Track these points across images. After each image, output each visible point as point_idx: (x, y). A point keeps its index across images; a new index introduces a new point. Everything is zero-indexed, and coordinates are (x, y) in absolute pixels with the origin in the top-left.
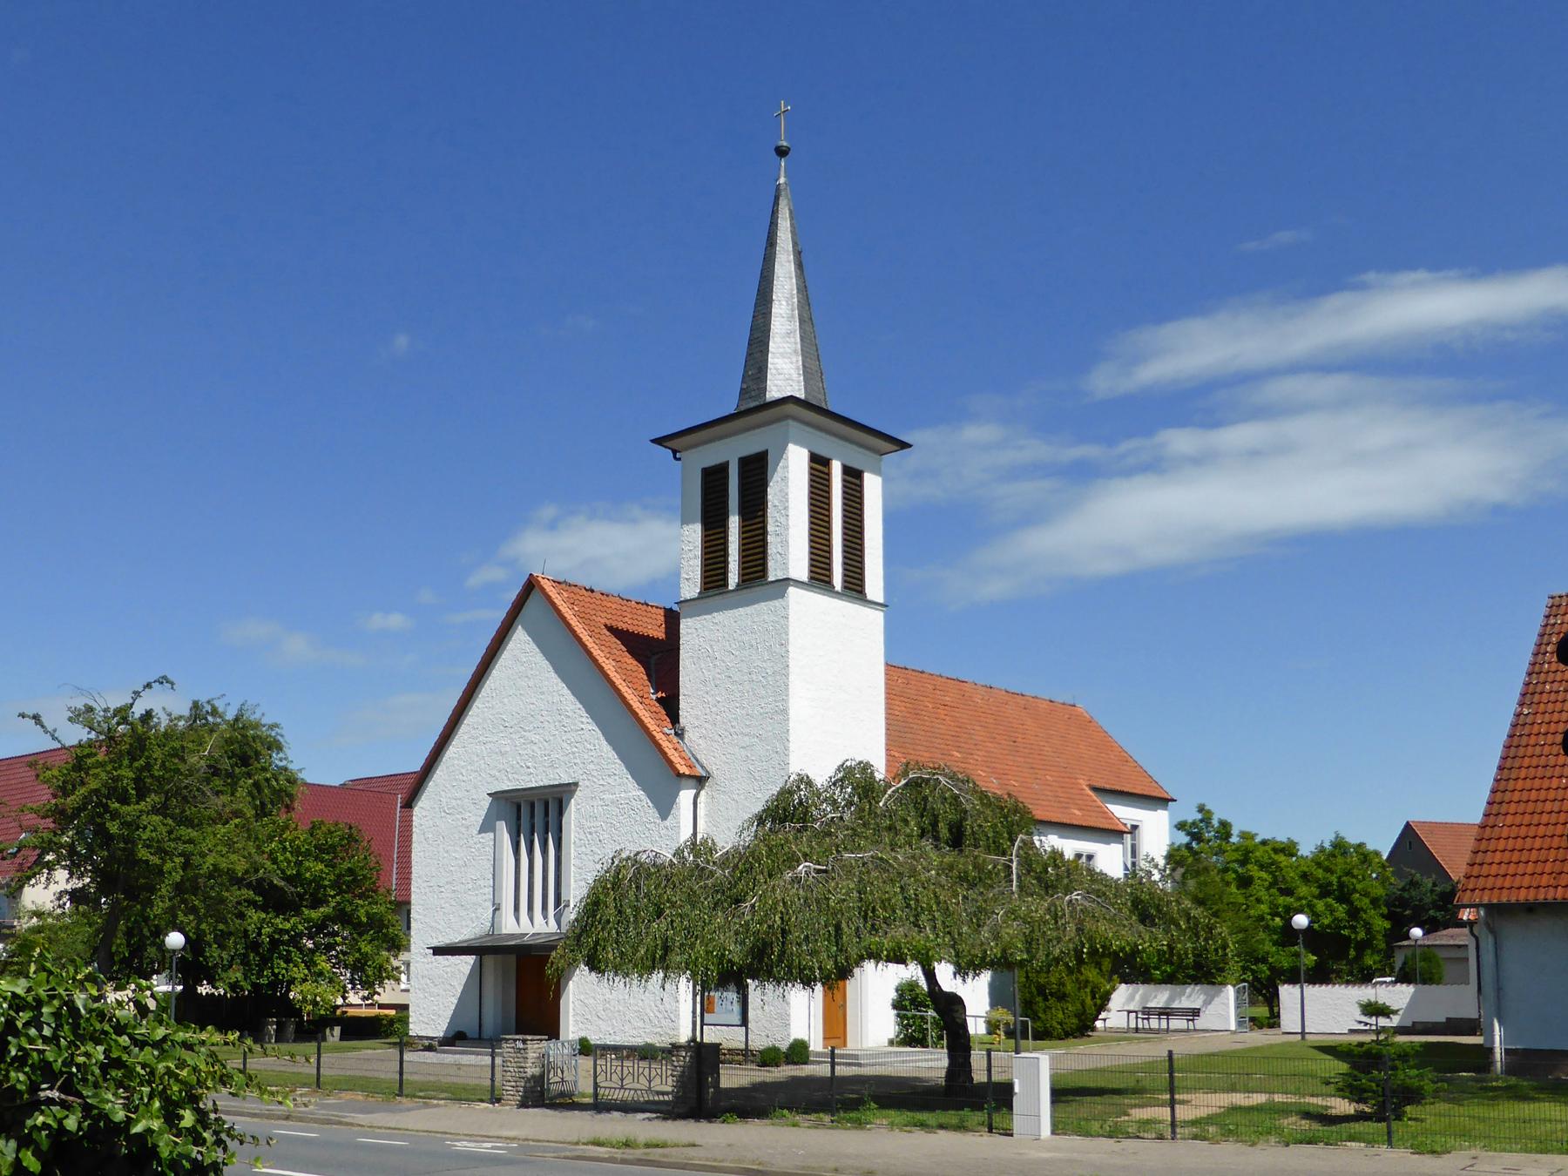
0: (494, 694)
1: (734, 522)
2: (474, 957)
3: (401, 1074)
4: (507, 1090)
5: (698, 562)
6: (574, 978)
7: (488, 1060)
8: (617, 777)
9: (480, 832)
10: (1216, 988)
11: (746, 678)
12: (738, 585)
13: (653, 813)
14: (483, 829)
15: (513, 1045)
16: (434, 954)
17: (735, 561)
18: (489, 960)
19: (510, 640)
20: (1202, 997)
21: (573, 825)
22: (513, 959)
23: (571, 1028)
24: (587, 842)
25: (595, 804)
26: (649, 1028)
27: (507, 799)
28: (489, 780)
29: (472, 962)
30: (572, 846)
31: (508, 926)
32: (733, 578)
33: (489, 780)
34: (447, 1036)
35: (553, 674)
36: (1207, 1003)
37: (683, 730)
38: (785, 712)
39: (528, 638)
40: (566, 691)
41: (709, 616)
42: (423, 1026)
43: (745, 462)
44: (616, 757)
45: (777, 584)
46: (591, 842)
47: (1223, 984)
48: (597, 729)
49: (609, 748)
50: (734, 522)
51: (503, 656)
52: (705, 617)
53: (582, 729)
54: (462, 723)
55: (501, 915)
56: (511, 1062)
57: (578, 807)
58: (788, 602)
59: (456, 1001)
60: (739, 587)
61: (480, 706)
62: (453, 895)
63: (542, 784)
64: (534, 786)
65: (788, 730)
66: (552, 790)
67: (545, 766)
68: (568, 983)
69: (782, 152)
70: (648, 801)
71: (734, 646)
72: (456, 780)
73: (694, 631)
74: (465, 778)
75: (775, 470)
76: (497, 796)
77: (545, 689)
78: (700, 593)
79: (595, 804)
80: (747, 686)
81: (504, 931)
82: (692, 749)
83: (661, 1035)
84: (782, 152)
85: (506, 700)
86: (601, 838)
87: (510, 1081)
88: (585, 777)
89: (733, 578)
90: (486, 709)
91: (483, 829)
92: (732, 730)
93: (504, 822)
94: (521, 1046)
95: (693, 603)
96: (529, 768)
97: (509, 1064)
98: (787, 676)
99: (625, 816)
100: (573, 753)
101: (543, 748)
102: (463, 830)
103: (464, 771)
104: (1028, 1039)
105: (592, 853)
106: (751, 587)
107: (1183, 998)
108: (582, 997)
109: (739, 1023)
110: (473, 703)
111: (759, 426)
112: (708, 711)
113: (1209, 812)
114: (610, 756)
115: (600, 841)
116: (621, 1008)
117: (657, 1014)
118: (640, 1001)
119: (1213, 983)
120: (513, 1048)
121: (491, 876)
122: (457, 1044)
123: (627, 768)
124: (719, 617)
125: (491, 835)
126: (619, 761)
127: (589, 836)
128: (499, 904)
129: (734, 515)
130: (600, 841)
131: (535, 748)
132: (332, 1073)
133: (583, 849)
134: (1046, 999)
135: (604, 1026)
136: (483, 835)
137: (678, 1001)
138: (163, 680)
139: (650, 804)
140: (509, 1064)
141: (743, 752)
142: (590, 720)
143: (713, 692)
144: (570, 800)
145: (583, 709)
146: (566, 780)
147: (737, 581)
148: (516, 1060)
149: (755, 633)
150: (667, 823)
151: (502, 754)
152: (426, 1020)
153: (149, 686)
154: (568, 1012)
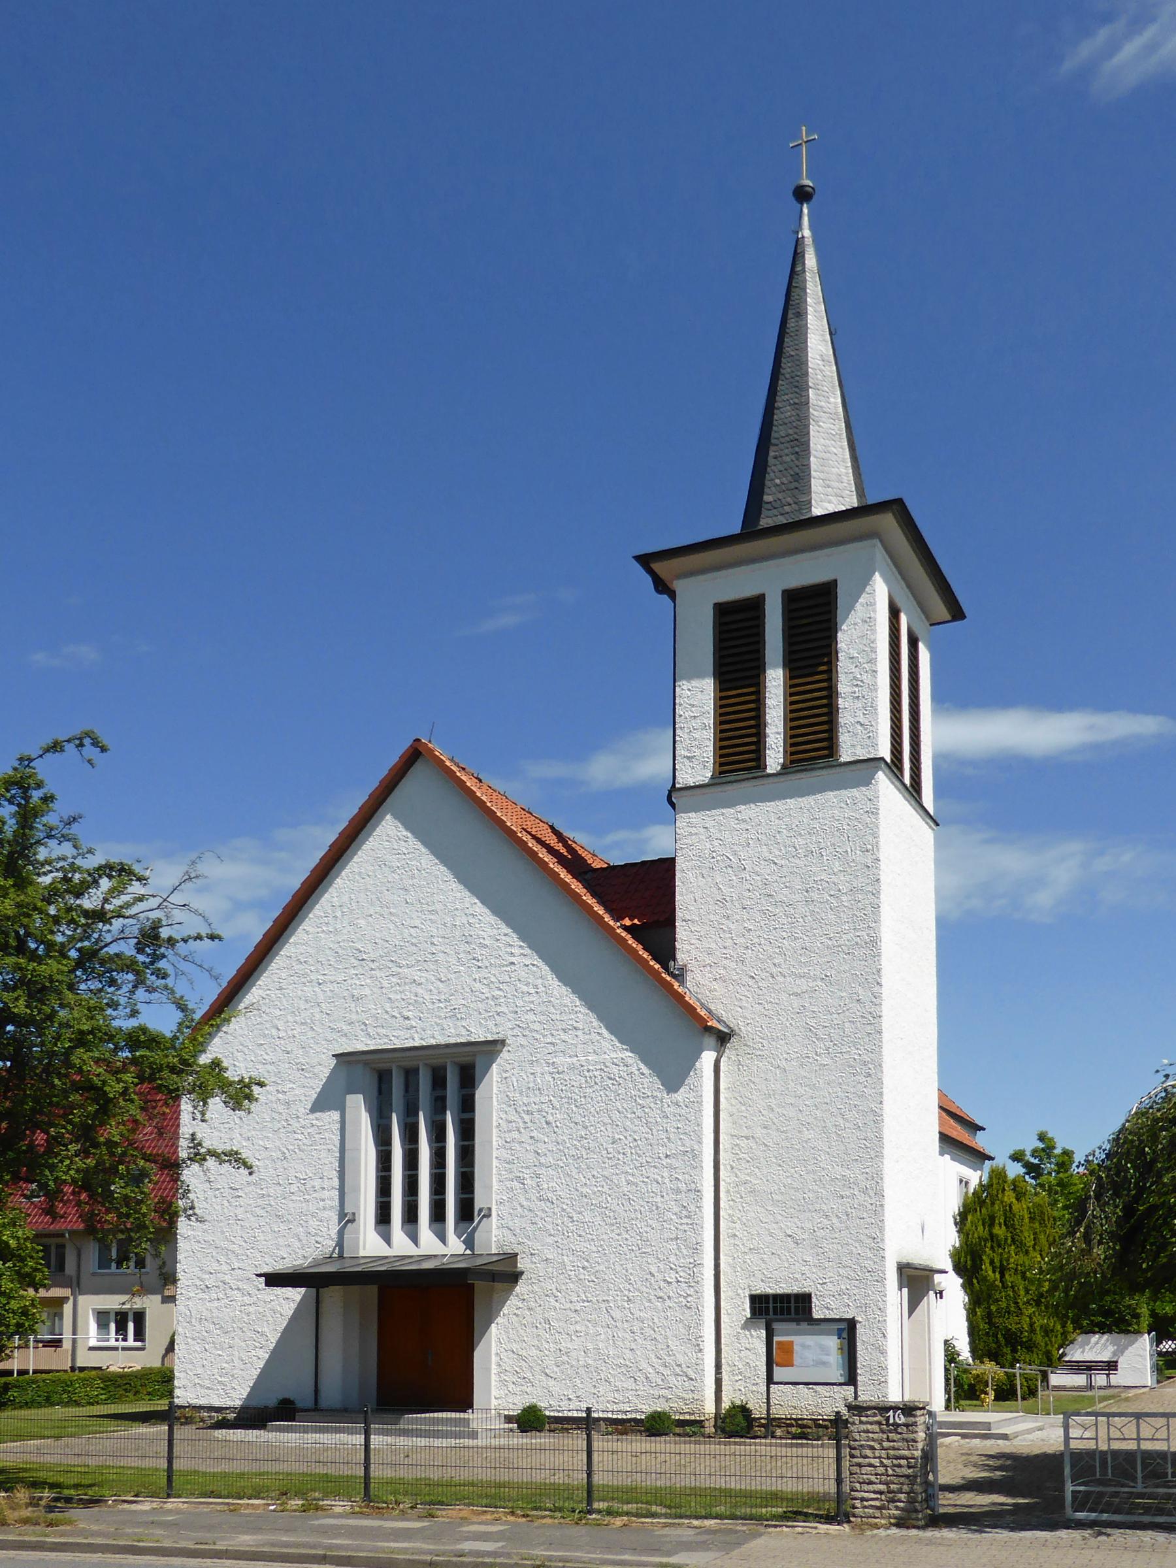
0: (339, 914)
1: (775, 680)
2: (303, 1290)
3: (589, 1475)
4: (863, 1499)
5: (709, 734)
6: (499, 1320)
7: (359, 1439)
8: (579, 1033)
9: (313, 1110)
10: (1132, 1337)
11: (798, 897)
12: (784, 766)
13: (650, 1082)
14: (319, 1105)
15: (878, 1418)
16: (268, 1284)
17: (778, 733)
18: (333, 1296)
19: (369, 835)
20: (1111, 1348)
21: (495, 1099)
22: (373, 1290)
23: (494, 1392)
24: (522, 1125)
25: (538, 1070)
26: (644, 1390)
27: (366, 1064)
28: (329, 1035)
29: (298, 1298)
30: (494, 1131)
31: (367, 1246)
32: (774, 758)
33: (329, 1035)
34: (254, 1404)
35: (454, 885)
36: (1121, 1351)
37: (683, 969)
38: (874, 944)
39: (405, 833)
40: (479, 908)
41: (731, 811)
42: (200, 1391)
43: (793, 599)
44: (578, 1003)
45: (853, 767)
46: (529, 1124)
47: (1138, 1332)
48: (540, 963)
49: (564, 990)
50: (775, 680)
51: (356, 859)
52: (724, 811)
53: (513, 963)
54: (277, 954)
55: (357, 1231)
56: (872, 1448)
57: (504, 1075)
58: (876, 791)
59: (267, 1356)
60: (786, 769)
61: (310, 929)
62: (260, 1201)
63: (433, 1042)
64: (416, 1044)
65: (879, 971)
66: (404, 1054)
67: (440, 1017)
68: (488, 1326)
69: (802, 195)
70: (642, 1066)
71: (777, 853)
72: (265, 1036)
73: (702, 830)
74: (282, 1034)
75: (851, 607)
76: (344, 1059)
77: (438, 906)
78: (713, 777)
79: (538, 1070)
80: (802, 909)
81: (362, 1253)
82: (699, 996)
83: (667, 1400)
84: (802, 195)
85: (362, 922)
86: (550, 1118)
87: (871, 1483)
88: (516, 1031)
89: (774, 758)
90: (322, 935)
91: (319, 1105)
92: (774, 970)
93: (361, 1097)
94: (902, 1420)
95: (698, 791)
96: (408, 1018)
97: (868, 1452)
98: (876, 894)
99: (596, 1087)
100: (494, 998)
101: (435, 991)
102: (281, 1108)
103: (280, 1024)
104: (1017, 1400)
105: (531, 1141)
106: (812, 769)
107: (1087, 1348)
108: (515, 1347)
109: (842, 1380)
110: (299, 925)
111: (802, 550)
112: (729, 943)
113: (1051, 1139)
114: (567, 1001)
115: (547, 1123)
116: (590, 1362)
117: (662, 1369)
118: (627, 1351)
119: (1127, 1332)
120: (880, 1423)
121: (335, 1174)
122: (297, 1417)
123: (601, 1018)
124: (747, 811)
125: (336, 1115)
126: (584, 1010)
127: (527, 1118)
128: (354, 1214)
129: (775, 667)
130: (547, 1123)
131: (420, 991)
132: (389, 1473)
133: (515, 1135)
134: (1014, 1351)
135: (556, 1388)
136: (318, 1114)
137: (700, 1351)
138: (86, 739)
139: (645, 1070)
140: (868, 1452)
141: (796, 1002)
142: (528, 951)
143: (738, 917)
144: (490, 1066)
145: (514, 935)
146: (479, 1035)
147: (781, 761)
148: (886, 1444)
149: (817, 834)
150: (680, 1096)
151: (356, 999)
152: (207, 1383)
153: (55, 747)
154: (489, 1370)
